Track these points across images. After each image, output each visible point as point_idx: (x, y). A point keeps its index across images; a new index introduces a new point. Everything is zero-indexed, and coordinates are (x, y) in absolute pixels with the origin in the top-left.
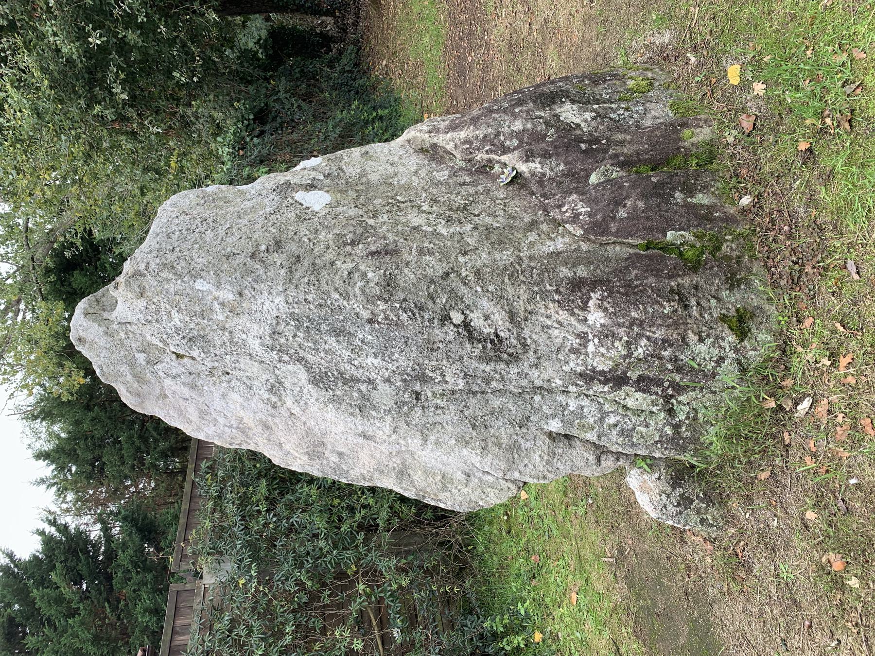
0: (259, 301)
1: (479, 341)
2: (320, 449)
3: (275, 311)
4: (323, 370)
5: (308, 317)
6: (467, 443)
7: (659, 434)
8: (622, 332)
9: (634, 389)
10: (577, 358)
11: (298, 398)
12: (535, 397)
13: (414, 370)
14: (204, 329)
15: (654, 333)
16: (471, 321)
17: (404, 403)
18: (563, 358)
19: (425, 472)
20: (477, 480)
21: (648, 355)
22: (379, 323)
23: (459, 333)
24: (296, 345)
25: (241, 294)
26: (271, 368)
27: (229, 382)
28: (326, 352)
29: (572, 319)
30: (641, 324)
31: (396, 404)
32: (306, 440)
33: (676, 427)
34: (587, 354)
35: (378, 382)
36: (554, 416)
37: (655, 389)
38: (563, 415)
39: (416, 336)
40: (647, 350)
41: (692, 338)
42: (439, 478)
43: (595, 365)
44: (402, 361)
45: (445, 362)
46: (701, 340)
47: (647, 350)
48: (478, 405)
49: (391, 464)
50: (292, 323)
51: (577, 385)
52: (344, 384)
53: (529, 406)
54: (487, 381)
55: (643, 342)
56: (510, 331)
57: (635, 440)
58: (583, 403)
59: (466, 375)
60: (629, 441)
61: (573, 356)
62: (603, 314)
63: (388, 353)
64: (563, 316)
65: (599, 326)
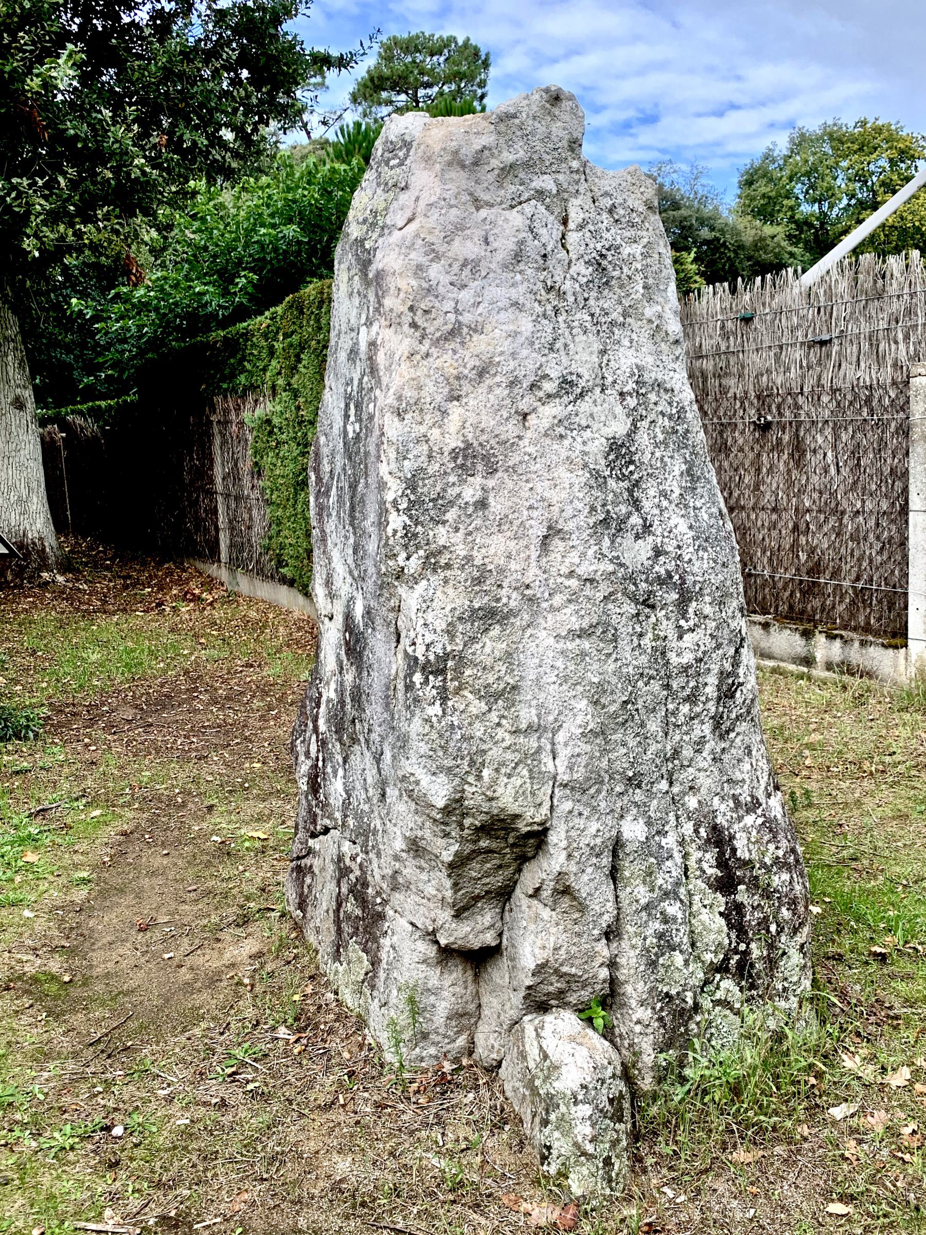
0: (676, 366)
2: (480, 467)
4: (636, 457)
5: (687, 431)
8: (784, 844)
9: (722, 909)
10: (732, 810)
11: (566, 423)
14: (621, 287)
19: (509, 654)
20: (536, 745)
24: (652, 416)
26: (598, 381)
27: (545, 316)
29: (766, 778)
32: (493, 442)
35: (650, 539)
36: (649, 824)
37: (733, 935)
43: (738, 836)
45: (714, 624)
49: (504, 592)
50: (674, 411)
51: (696, 831)
52: (628, 490)
54: (692, 699)
59: (701, 660)
60: (656, 954)
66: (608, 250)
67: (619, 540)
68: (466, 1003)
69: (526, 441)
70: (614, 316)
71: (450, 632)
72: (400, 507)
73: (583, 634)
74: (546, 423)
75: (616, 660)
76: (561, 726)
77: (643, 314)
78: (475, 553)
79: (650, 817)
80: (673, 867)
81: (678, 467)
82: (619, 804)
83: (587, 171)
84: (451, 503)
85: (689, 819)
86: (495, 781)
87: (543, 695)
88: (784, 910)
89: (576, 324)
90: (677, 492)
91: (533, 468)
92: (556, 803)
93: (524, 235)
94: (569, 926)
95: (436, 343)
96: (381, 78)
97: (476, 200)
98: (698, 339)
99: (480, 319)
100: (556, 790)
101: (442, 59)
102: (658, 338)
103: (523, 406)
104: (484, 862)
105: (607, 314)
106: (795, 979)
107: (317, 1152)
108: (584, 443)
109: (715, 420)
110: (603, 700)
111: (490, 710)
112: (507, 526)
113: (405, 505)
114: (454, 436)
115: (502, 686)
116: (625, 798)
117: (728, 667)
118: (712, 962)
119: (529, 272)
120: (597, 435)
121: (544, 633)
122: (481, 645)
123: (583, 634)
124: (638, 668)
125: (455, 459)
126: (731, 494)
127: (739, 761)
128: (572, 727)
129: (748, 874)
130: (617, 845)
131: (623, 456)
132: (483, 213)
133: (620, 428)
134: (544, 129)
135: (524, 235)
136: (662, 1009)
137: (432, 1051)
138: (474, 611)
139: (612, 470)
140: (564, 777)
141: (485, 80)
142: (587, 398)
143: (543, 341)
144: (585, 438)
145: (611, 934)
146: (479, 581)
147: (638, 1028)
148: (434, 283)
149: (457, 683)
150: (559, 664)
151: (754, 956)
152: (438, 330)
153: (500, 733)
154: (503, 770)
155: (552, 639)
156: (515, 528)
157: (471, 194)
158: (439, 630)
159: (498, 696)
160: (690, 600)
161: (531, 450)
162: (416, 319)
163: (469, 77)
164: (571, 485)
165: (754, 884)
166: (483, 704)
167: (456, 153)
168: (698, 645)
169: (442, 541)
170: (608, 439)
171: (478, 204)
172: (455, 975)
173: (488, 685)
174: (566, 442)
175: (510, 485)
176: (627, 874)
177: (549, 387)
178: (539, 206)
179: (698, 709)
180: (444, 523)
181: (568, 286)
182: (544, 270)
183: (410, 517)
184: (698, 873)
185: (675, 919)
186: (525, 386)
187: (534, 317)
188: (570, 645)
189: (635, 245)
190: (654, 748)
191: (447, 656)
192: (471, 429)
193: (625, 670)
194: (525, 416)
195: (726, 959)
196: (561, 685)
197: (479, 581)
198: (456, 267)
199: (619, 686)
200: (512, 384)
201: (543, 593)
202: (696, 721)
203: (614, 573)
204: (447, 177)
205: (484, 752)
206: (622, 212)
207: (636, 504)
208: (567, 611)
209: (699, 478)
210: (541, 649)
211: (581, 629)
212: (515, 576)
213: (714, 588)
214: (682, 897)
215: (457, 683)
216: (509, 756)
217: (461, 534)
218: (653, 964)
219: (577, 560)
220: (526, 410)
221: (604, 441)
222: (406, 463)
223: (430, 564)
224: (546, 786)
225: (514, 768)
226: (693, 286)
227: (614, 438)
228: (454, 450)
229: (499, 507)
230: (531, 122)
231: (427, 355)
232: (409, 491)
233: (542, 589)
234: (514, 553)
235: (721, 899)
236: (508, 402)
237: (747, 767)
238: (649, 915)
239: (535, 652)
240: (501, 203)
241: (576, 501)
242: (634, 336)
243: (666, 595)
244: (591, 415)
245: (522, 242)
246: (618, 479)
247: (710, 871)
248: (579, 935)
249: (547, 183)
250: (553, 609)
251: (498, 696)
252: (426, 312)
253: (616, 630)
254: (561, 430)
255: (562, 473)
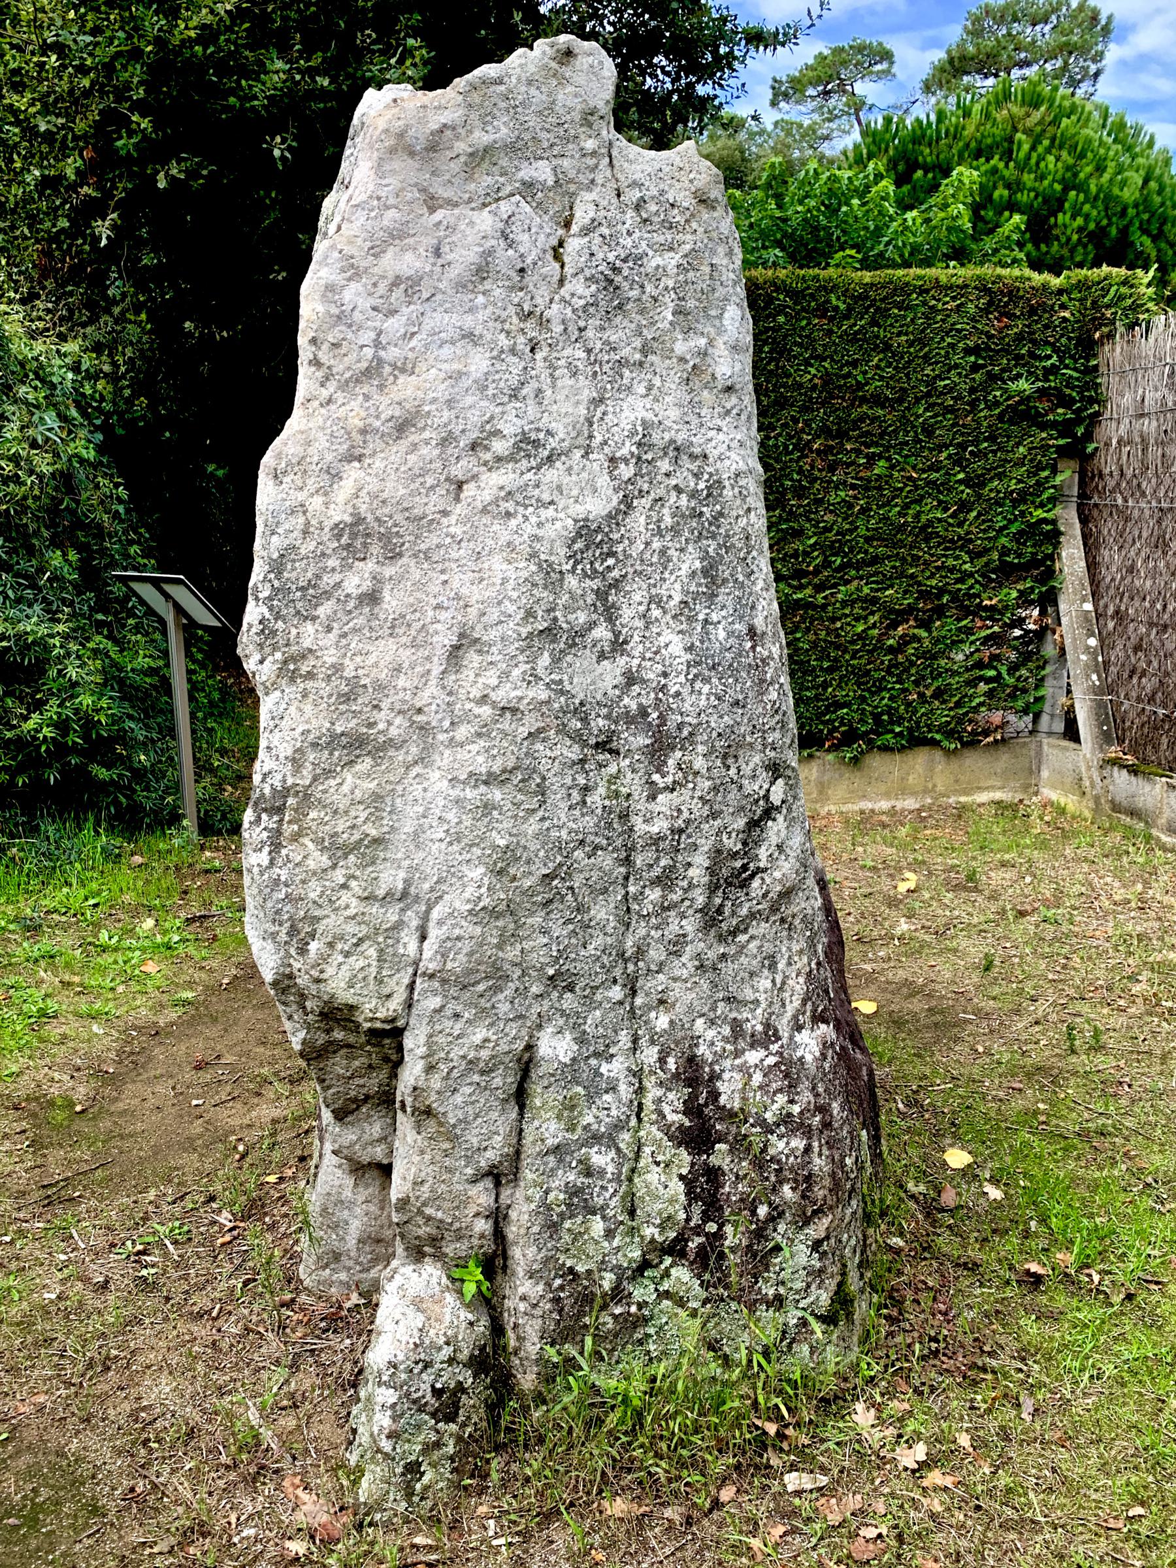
0: (722, 424)
1: (745, 844)
3: (716, 453)
4: (619, 548)
5: (721, 514)
6: (500, 872)
7: (593, 1266)
8: (806, 1097)
9: (684, 1171)
10: (726, 1040)
12: (618, 988)
13: (680, 727)
14: (642, 312)
15: (820, 1155)
16: (774, 820)
17: (585, 720)
18: (719, 1012)
19: (377, 797)
20: (395, 918)
21: (779, 1162)
22: (753, 648)
23: (757, 801)
24: (660, 492)
25: (729, 389)
26: (581, 441)
27: (513, 351)
28: (663, 552)
29: (797, 1003)
30: (827, 1125)
31: (582, 704)
32: (398, 517)
33: (618, 1294)
34: (737, 1054)
35: (622, 661)
36: (581, 1040)
37: (697, 1209)
38: (588, 1058)
39: (750, 720)
40: (787, 1157)
41: (817, 1230)
42: (374, 832)
43: (726, 1076)
44: (694, 703)
45: (708, 784)
46: (816, 1245)
47: (787, 1157)
48: (595, 875)
49: (381, 716)
50: (702, 485)
51: (662, 1061)
52: (597, 592)
53: (598, 981)
54: (665, 881)
55: (798, 1143)
56: (765, 896)
57: (567, 1224)
58: (622, 1087)
59: (681, 831)
61: (726, 1030)
62: (818, 1054)
63: (707, 673)
64: (798, 986)
65: (799, 1054)
66: (625, 261)
67: (569, 658)
68: (382, 1227)
69: (453, 519)
70: (625, 352)
71: (296, 761)
72: (261, 595)
73: (490, 780)
74: (487, 496)
75: (543, 819)
76: (441, 897)
77: (672, 350)
78: (347, 662)
79: (584, 1032)
80: (614, 1105)
81: (691, 562)
82: (535, 1009)
83: (614, 153)
84: (327, 595)
85: (652, 1042)
86: (324, 959)
87: (421, 855)
88: (786, 1188)
89: (562, 362)
90: (677, 598)
91: (454, 555)
92: (416, 997)
93: (493, 242)
94: (438, 1158)
95: (344, 386)
96: (963, 58)
97: (432, 198)
98: (1140, 392)
99: (410, 355)
100: (419, 981)
101: (1047, 28)
102: (696, 384)
103: (458, 471)
104: (350, 1058)
105: (615, 349)
106: (799, 1285)
107: (148, 1367)
108: (540, 525)
109: (1154, 504)
110: (512, 871)
111: (334, 866)
112: (404, 629)
113: (266, 594)
114: (341, 507)
115: (357, 836)
116: (546, 1003)
117: (732, 843)
118: (653, 1241)
119: (497, 292)
120: (562, 515)
121: (437, 774)
122: (338, 780)
123: (490, 780)
124: (577, 833)
125: (339, 537)
126: (1165, 607)
127: (752, 974)
128: (457, 900)
129: (734, 1129)
130: (526, 1063)
131: (599, 545)
132: (439, 215)
133: (597, 506)
134: (544, 97)
135: (493, 242)
136: (561, 1288)
137: (343, 1276)
138: (334, 737)
139: (576, 563)
140: (430, 964)
141: (1102, 52)
142: (558, 464)
143: (502, 384)
144: (543, 519)
145: (500, 1176)
146: (347, 698)
147: (522, 1306)
148: (347, 308)
149: (296, 827)
150: (451, 816)
151: (727, 1243)
152: (349, 368)
153: (345, 897)
154: (339, 946)
155: (446, 783)
156: (413, 633)
157: (423, 190)
158: (282, 756)
159: (348, 850)
160: (673, 749)
161: (457, 530)
162: (320, 355)
163: (1082, 50)
164: (504, 581)
165: (740, 1145)
166: (325, 858)
167: (401, 135)
168: (679, 811)
169: (307, 643)
170: (576, 521)
171: (432, 203)
172: (370, 1190)
173: (336, 833)
174: (513, 523)
175: (416, 574)
176: (538, 1102)
177: (500, 447)
178: (523, 204)
179: (674, 897)
180: (314, 619)
181: (554, 311)
182: (521, 289)
183: (271, 609)
184: (654, 1117)
185: (602, 1172)
186: (462, 444)
187: (495, 353)
188: (469, 793)
189: (672, 254)
190: (598, 941)
191: (285, 792)
192: (367, 500)
193: (554, 834)
194: (460, 485)
195: (681, 1239)
196: (451, 843)
197: (347, 698)
198: (382, 288)
199: (542, 853)
200: (444, 442)
201: (441, 721)
202: (672, 913)
203: (548, 702)
204: (388, 168)
205: (318, 919)
206: (653, 208)
207: (610, 614)
208: (474, 748)
209: (725, 581)
210: (429, 795)
211: (490, 774)
212: (401, 695)
213: (714, 734)
214: (622, 1146)
215: (296, 827)
216: (351, 928)
217: (333, 636)
218: (553, 1227)
219: (494, 681)
220: (460, 477)
221: (570, 522)
222: (275, 538)
223: (288, 670)
224: (403, 973)
225: (357, 945)
226: (1141, 317)
227: (586, 520)
228: (337, 525)
229: (394, 603)
230: (523, 89)
231: (329, 401)
232: (272, 576)
233: (439, 716)
234: (406, 665)
235: (685, 1156)
236: (438, 465)
237: (765, 983)
238: (560, 1161)
239: (419, 797)
240: (470, 200)
241: (507, 603)
242: (657, 382)
243: (631, 739)
244: (559, 488)
245: (490, 252)
246: (585, 575)
247: (672, 1117)
248: (449, 1170)
249: (542, 171)
250: (452, 743)
251: (348, 850)
252: (335, 345)
253: (544, 778)
254: (510, 506)
255: (497, 565)
